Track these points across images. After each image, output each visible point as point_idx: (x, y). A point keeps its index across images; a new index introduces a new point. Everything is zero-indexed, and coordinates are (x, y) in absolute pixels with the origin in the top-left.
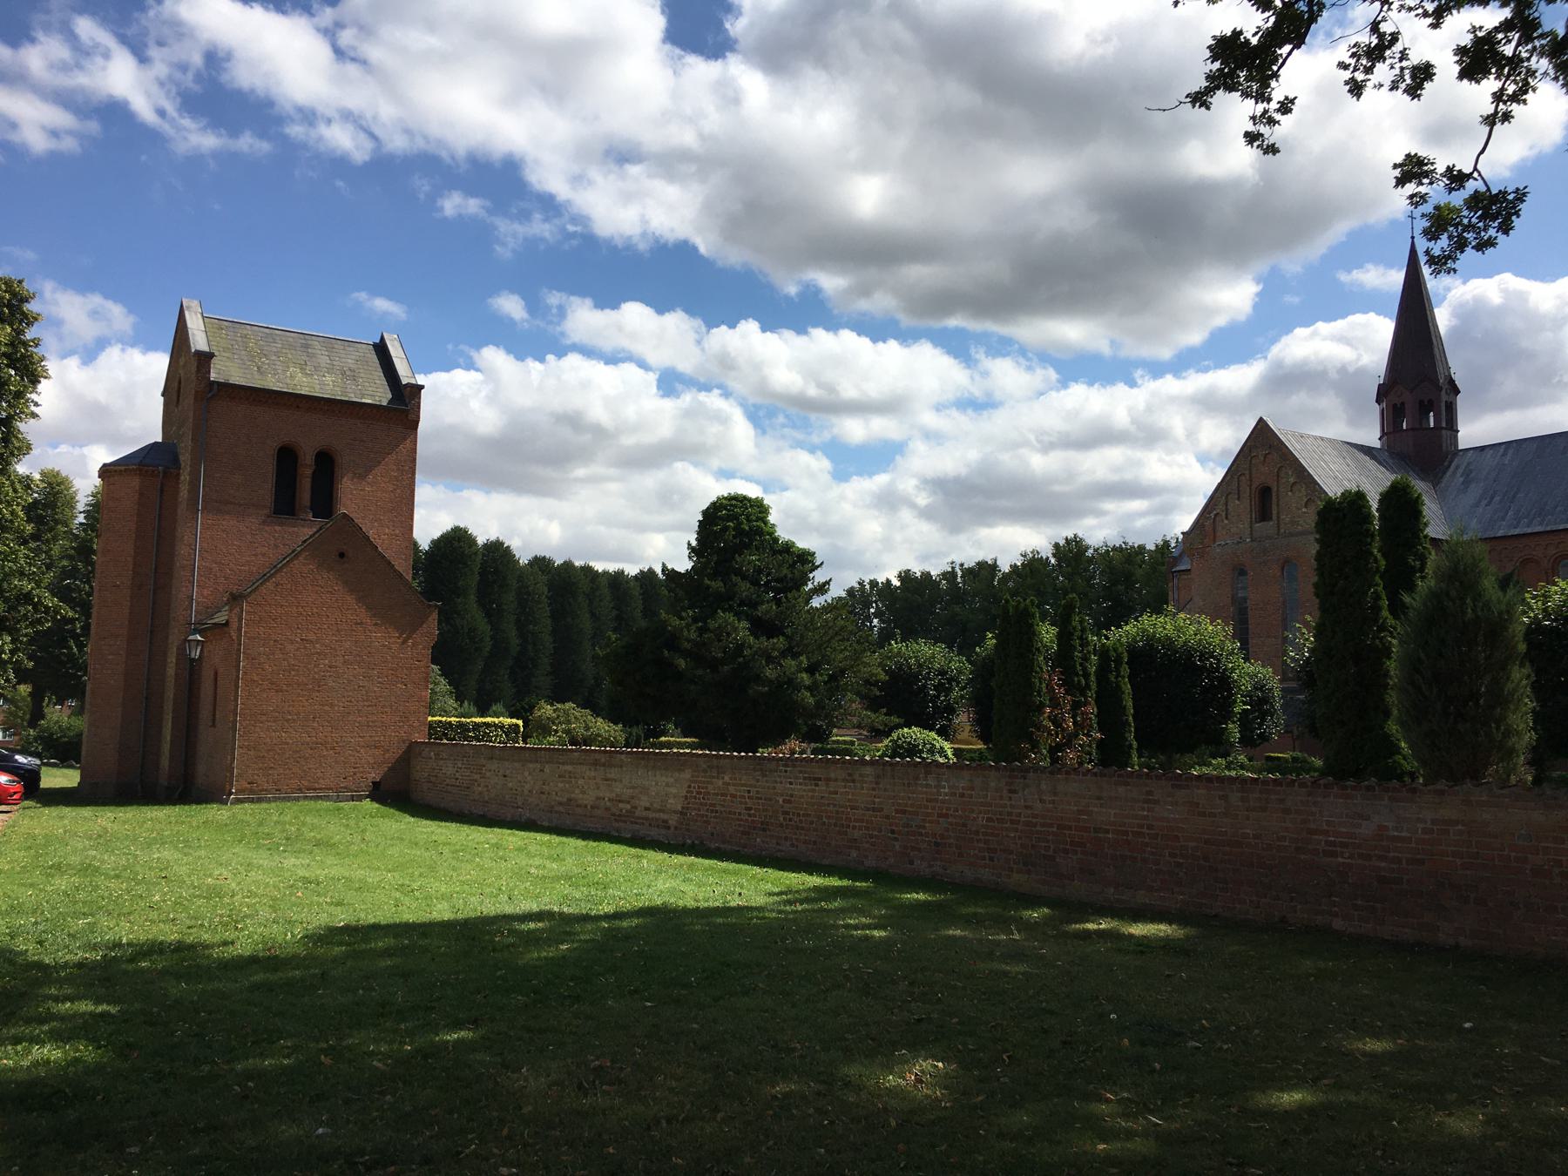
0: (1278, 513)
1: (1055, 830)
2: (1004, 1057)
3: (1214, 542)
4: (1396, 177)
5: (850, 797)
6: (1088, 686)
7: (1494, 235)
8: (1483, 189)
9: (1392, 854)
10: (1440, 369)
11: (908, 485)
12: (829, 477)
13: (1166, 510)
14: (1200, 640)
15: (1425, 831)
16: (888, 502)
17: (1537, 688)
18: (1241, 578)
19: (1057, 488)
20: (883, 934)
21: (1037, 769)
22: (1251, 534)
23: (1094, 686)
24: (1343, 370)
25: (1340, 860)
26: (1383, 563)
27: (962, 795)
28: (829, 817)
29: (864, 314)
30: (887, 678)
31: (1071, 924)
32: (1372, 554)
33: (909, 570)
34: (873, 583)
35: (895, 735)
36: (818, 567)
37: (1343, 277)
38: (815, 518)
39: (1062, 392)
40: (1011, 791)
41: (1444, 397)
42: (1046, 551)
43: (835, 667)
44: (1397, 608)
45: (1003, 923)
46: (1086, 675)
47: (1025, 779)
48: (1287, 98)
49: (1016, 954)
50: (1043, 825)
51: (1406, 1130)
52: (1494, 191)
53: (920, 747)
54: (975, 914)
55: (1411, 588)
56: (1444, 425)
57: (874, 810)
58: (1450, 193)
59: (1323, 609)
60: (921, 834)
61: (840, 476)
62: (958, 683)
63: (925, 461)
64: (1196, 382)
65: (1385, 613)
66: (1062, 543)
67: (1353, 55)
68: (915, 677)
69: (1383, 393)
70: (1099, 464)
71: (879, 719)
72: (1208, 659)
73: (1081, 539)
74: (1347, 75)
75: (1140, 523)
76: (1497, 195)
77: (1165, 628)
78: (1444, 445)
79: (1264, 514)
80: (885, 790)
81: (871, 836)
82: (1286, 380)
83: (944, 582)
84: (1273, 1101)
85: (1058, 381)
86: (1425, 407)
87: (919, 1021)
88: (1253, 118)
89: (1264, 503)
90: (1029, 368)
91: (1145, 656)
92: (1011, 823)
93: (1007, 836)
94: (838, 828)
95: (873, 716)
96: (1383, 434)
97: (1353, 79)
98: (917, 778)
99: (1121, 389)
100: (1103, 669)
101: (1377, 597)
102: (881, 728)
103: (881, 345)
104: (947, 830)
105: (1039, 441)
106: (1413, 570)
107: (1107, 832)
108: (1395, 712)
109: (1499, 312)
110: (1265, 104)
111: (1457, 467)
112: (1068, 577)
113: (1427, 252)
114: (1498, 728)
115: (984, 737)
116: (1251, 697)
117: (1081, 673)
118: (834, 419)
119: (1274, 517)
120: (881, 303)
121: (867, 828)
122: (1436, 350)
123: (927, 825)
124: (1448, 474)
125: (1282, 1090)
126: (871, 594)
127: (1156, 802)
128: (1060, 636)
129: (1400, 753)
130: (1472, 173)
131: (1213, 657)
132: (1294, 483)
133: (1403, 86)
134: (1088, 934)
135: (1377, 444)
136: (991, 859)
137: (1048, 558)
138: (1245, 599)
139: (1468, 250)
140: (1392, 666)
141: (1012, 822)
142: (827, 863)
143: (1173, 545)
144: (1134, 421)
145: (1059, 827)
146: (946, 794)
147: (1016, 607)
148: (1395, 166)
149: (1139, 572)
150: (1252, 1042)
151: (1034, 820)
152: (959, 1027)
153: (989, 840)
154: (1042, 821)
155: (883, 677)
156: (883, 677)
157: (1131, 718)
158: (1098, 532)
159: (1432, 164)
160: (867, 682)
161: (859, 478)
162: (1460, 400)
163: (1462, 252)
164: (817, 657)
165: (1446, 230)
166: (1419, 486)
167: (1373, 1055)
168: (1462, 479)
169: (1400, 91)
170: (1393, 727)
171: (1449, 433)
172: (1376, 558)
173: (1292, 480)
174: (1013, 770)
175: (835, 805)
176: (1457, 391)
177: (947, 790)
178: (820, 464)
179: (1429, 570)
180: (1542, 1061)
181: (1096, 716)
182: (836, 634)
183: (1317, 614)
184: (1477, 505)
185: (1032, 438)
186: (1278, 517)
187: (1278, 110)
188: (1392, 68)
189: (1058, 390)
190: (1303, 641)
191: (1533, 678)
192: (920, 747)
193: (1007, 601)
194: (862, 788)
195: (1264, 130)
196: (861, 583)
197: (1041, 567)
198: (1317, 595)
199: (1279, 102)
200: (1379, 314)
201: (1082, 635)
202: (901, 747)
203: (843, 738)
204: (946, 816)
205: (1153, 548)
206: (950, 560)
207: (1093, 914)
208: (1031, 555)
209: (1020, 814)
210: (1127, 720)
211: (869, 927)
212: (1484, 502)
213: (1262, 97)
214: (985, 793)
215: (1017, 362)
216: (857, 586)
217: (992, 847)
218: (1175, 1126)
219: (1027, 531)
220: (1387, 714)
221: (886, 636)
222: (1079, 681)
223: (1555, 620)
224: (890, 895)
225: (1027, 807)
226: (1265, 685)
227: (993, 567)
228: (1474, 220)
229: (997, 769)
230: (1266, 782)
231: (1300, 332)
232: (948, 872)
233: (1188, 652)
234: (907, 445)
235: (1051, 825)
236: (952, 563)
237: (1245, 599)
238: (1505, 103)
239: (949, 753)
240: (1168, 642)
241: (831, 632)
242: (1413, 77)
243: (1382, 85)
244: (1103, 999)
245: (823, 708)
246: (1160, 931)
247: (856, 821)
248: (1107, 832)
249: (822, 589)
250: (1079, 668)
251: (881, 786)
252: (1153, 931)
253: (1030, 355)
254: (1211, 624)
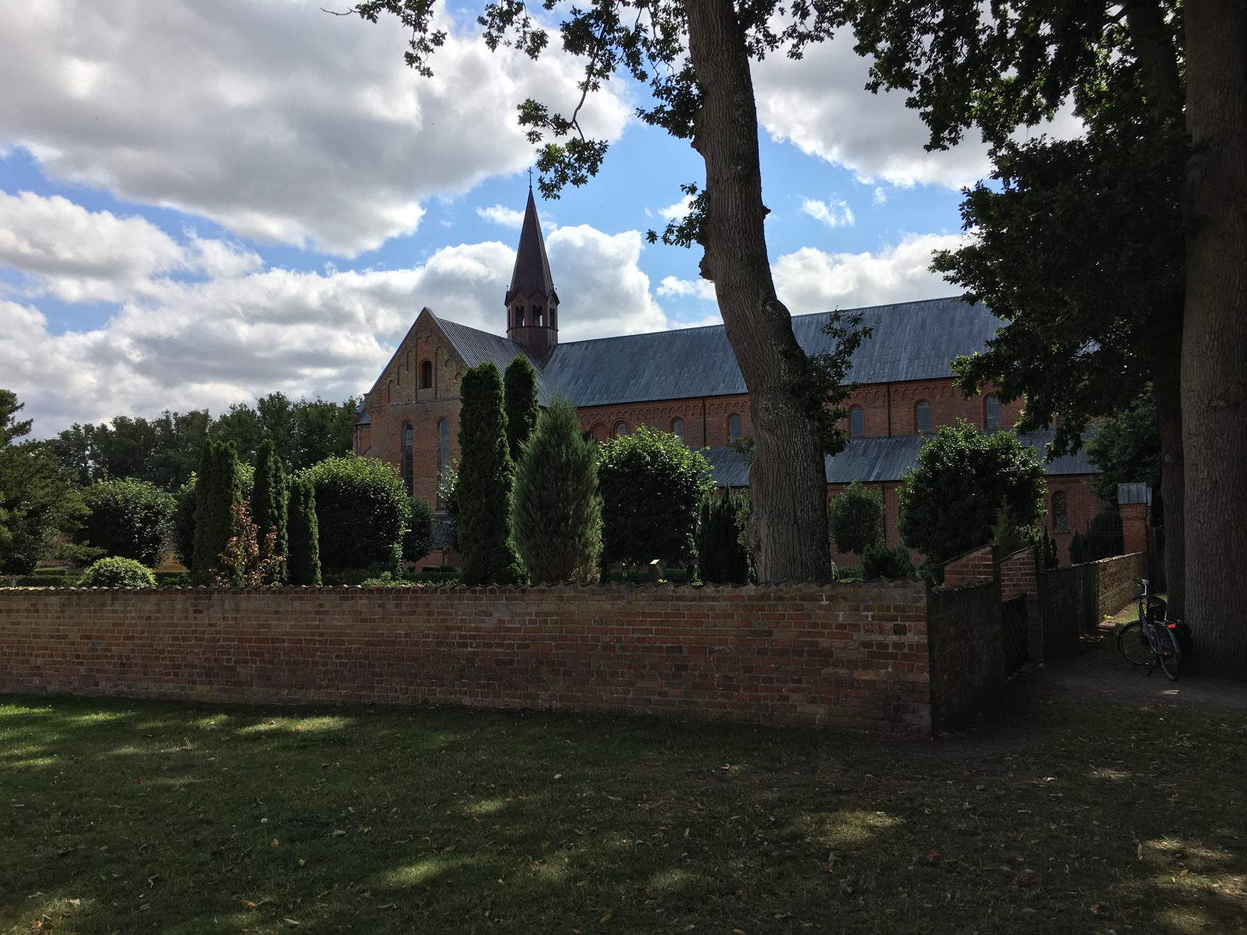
0: (436, 383)
1: (236, 643)
2: (150, 881)
4: (520, 116)
5: (33, 626)
6: (280, 517)
7: (585, 174)
8: (579, 137)
9: (507, 642)
10: (547, 285)
11: (122, 343)
12: (43, 330)
13: (352, 377)
14: (374, 478)
15: (531, 622)
16: (103, 356)
17: (604, 513)
18: (408, 431)
19: (261, 354)
20: (48, 761)
21: (220, 591)
22: (416, 397)
23: (285, 516)
24: (479, 281)
25: (469, 649)
26: (507, 419)
27: (149, 618)
28: (9, 647)
29: (79, 185)
30: (92, 512)
31: (245, 727)
32: (499, 412)
33: (125, 418)
34: (89, 428)
35: (96, 565)
36: (18, 408)
37: (480, 212)
38: (28, 366)
39: (264, 275)
40: (195, 612)
41: (549, 305)
42: (253, 405)
43: (36, 503)
44: (516, 453)
45: (176, 734)
46: (279, 507)
47: (210, 599)
48: (439, 32)
49: (185, 765)
50: (226, 640)
51: (509, 885)
52: (586, 141)
53: (122, 575)
54: (152, 729)
55: (525, 438)
56: (549, 325)
57: (59, 637)
58: (557, 135)
59: (464, 453)
60: (107, 657)
61: (55, 329)
62: (164, 516)
63: (136, 321)
64: (373, 278)
65: (508, 457)
66: (267, 398)
67: (490, 14)
68: (122, 512)
69: (509, 299)
70: (297, 336)
71: (82, 550)
72: (379, 493)
73: (283, 396)
74: (485, 29)
75: (332, 386)
76: (588, 144)
77: (346, 469)
78: (549, 340)
79: (426, 383)
80: (71, 618)
81: (55, 663)
82: (440, 283)
83: (158, 429)
84: (402, 878)
85: (264, 266)
86: (537, 311)
87: (63, 855)
88: (413, 43)
89: (426, 373)
90: (237, 252)
91: (329, 492)
92: (196, 640)
93: (192, 652)
94: (19, 658)
95: (75, 548)
96: (510, 328)
97: (489, 33)
98: (104, 605)
99: (314, 276)
100: (294, 502)
101: (503, 446)
102: (84, 558)
103: (95, 215)
104: (133, 651)
105: (245, 314)
106: (527, 426)
107: (284, 641)
108: (513, 531)
109: (582, 251)
110: (422, 33)
111: (557, 356)
112: (272, 427)
113: (541, 180)
114: (580, 541)
115: (187, 563)
116: (413, 522)
117: (274, 505)
118: (49, 278)
119: (433, 385)
120: (98, 176)
121: (51, 656)
122: (545, 270)
123: (113, 648)
124: (552, 359)
125: (410, 864)
126: (86, 438)
127: (327, 613)
128: (257, 476)
129: (515, 562)
130: (572, 123)
131: (384, 491)
133: (525, 46)
134: (258, 736)
135: (505, 336)
136: (176, 675)
137: (254, 411)
138: (410, 447)
139: (568, 183)
140: (512, 497)
141: (196, 639)
142: (8, 692)
143: (358, 404)
144: (325, 304)
145: (241, 641)
146: (133, 618)
147: (217, 449)
148: (519, 107)
149: (330, 425)
150: (390, 821)
151: (217, 636)
152: (106, 854)
153: (174, 657)
154: (225, 636)
155: (88, 511)
156: (88, 511)
157: (316, 542)
158: (297, 391)
159: (545, 110)
160: (72, 517)
161: (73, 333)
162: (560, 309)
163: (564, 184)
164: (14, 494)
165: (553, 165)
166: (532, 366)
167: (488, 816)
168: (559, 365)
169: (523, 50)
170: (511, 542)
171: (552, 331)
172: (502, 415)
173: (446, 358)
174: (198, 592)
175: (16, 636)
176: (557, 302)
177: (134, 614)
178: (35, 318)
179: (538, 426)
180: (609, 800)
181: (287, 542)
182: (38, 471)
183: (461, 457)
184: (569, 384)
185: (239, 309)
186: (436, 386)
187: (432, 41)
188: (518, 31)
189: (261, 273)
190: (450, 478)
191: (603, 505)
192: (122, 575)
193: (209, 444)
194: (46, 617)
195: (422, 55)
196: (76, 428)
197: (248, 418)
198: (460, 442)
199: (433, 34)
200: (504, 243)
201: (276, 474)
202: (103, 575)
203: (53, 569)
204: (132, 638)
205: (342, 406)
206: (164, 410)
207: (266, 716)
208: (239, 408)
209: (205, 631)
210: (313, 544)
211: (35, 756)
212: (573, 382)
213: (419, 26)
214: (171, 615)
215: (227, 246)
216: (72, 430)
217: (177, 663)
218: (311, 923)
219: (235, 388)
220: (507, 533)
221: (98, 474)
222: (272, 512)
223: (616, 464)
224: (68, 719)
225: (211, 625)
226: (424, 514)
227: (205, 417)
228: (572, 160)
229: (183, 592)
230: (415, 591)
231: (449, 250)
232: (133, 689)
233: (365, 488)
234: (122, 308)
235: (234, 640)
236: (167, 412)
237: (410, 447)
238: (594, 75)
239: (152, 578)
240: (349, 480)
241: (31, 470)
242: (533, 40)
243: (510, 43)
244: (260, 800)
245: (23, 542)
246: (324, 724)
247: (39, 649)
248: (284, 641)
249: (23, 428)
250: (273, 501)
251: (66, 614)
252: (317, 725)
253: (237, 240)
254: (383, 465)
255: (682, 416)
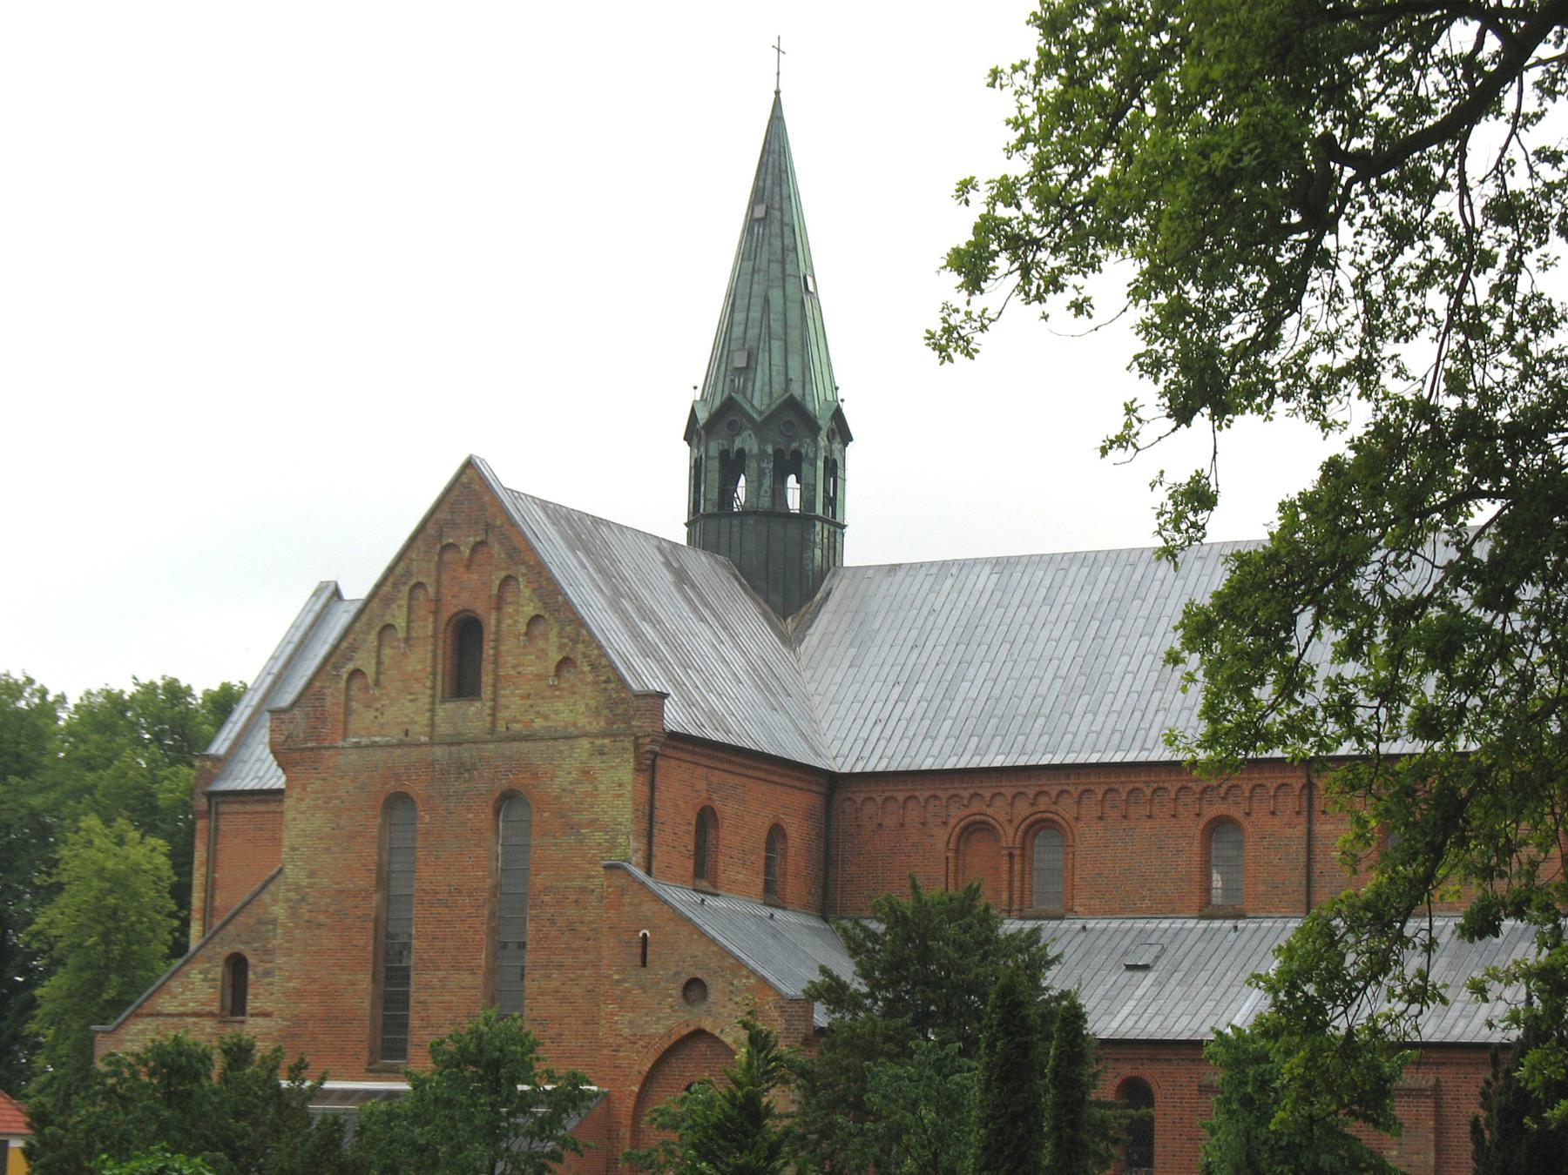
3: (345, 736)
56: (819, 511)
119: (487, 692)
132: (535, 619)
150: (1202, 363)
255: (1237, 813)
